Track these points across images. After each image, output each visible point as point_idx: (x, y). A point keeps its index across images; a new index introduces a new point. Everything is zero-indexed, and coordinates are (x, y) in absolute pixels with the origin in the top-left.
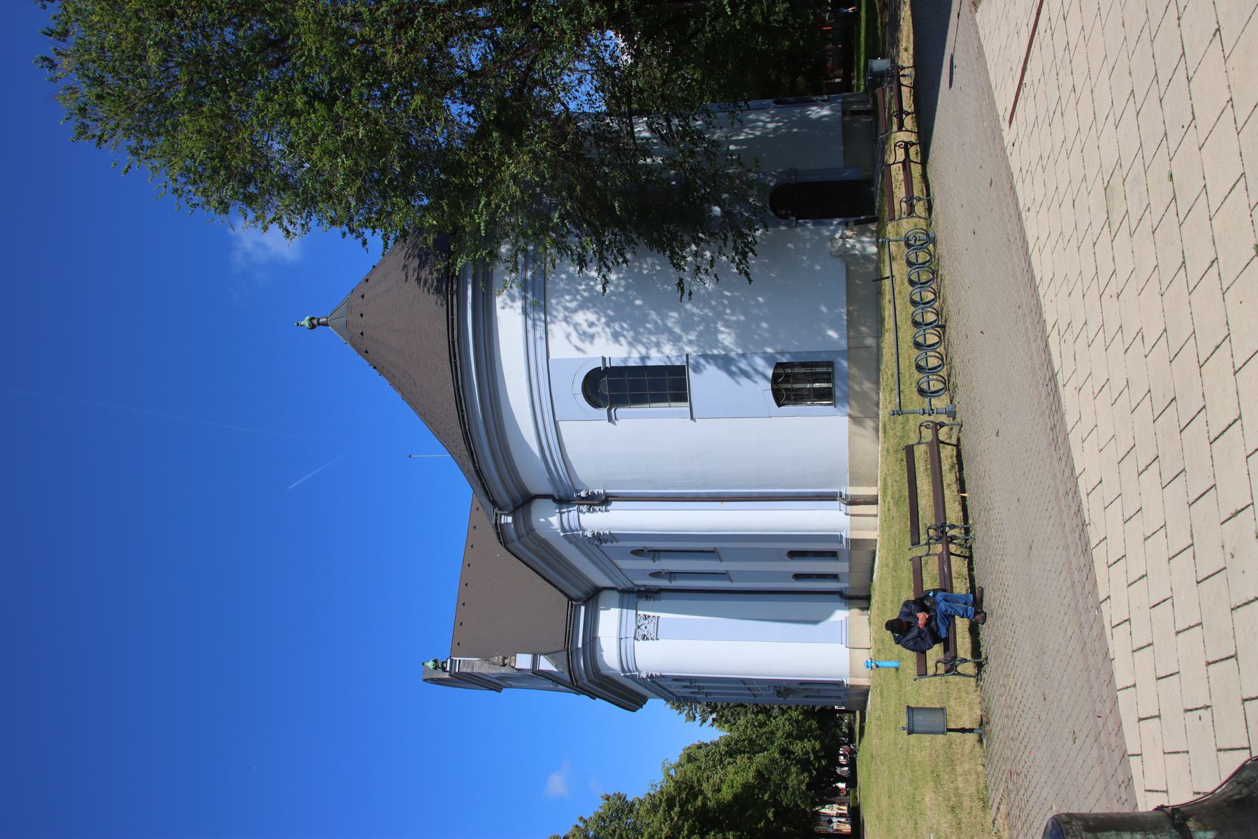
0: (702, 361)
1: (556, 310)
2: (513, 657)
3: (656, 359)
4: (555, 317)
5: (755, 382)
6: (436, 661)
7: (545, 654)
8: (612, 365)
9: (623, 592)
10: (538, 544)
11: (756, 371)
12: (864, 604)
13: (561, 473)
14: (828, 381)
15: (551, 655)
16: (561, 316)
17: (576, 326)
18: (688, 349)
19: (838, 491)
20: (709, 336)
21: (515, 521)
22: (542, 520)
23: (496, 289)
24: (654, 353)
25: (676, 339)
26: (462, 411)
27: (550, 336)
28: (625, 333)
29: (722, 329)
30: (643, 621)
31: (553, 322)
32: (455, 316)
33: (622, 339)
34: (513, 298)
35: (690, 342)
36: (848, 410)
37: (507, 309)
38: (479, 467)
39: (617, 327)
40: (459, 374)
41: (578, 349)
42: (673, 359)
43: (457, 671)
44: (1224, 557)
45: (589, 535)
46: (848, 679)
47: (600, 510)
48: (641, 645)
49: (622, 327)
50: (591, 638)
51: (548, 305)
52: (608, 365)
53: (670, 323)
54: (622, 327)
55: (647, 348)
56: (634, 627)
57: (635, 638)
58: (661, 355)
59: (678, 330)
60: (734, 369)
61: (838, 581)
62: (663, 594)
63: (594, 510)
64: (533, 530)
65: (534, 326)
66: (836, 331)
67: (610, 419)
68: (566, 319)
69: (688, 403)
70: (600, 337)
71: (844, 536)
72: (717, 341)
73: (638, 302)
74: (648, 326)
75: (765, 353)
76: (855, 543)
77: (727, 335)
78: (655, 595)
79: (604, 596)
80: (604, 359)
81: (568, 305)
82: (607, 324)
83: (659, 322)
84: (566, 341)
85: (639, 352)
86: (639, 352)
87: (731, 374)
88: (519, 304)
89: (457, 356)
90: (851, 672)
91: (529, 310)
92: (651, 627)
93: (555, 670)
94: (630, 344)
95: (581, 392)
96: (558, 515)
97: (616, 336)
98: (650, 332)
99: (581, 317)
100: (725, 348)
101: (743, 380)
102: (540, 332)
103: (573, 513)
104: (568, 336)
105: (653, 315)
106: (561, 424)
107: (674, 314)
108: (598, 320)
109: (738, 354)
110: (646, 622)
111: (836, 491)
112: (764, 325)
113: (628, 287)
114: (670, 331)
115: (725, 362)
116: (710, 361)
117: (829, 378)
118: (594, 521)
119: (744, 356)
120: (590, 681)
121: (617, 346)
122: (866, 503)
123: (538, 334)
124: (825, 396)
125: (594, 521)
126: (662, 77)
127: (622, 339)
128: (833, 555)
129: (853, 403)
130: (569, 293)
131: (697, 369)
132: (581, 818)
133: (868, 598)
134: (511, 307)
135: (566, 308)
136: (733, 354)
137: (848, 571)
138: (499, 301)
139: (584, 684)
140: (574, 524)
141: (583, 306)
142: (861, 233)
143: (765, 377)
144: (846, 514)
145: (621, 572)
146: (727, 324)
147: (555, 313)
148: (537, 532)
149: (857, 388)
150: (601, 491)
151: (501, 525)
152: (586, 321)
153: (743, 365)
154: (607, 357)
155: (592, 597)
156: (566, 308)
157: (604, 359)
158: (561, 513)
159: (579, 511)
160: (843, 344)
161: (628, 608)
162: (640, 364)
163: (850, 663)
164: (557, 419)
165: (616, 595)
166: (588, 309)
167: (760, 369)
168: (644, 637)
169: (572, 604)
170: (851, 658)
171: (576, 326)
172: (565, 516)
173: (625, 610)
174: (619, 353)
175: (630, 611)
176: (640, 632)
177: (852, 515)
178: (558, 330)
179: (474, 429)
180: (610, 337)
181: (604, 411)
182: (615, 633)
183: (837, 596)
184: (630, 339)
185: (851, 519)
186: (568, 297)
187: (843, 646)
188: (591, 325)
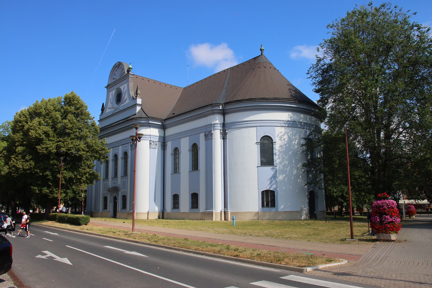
0: (275, 170)
1: (288, 130)
2: (140, 97)
3: (276, 158)
4: (286, 129)
5: (269, 185)
6: (132, 69)
7: (142, 108)
11: (272, 186)
12: (161, 217)
14: (266, 206)
16: (286, 131)
17: (284, 135)
18: (278, 167)
20: (283, 172)
21: (220, 110)
22: (217, 118)
23: (293, 113)
24: (277, 157)
25: (280, 163)
27: (281, 127)
28: (282, 149)
29: (283, 176)
30: (155, 143)
31: (285, 129)
32: (289, 101)
33: (280, 148)
34: (291, 117)
35: (280, 167)
36: (260, 211)
37: (288, 116)
39: (284, 147)
41: (278, 135)
42: (275, 162)
44: (385, 279)
45: (212, 132)
47: (221, 136)
48: (148, 142)
49: (284, 148)
51: (289, 128)
52: (274, 143)
53: (285, 161)
54: (284, 148)
55: (278, 155)
56: (154, 140)
57: (150, 141)
58: (277, 159)
59: (283, 164)
60: (273, 179)
62: (163, 151)
63: (221, 134)
64: (213, 114)
65: (286, 123)
66: (283, 208)
67: (257, 143)
68: (285, 132)
70: (281, 142)
72: (280, 175)
73: (290, 153)
74: (284, 156)
75: (277, 188)
76: (212, 213)
77: (282, 177)
79: (162, 131)
80: (275, 142)
81: (289, 133)
82: (285, 144)
83: (285, 159)
84: (280, 132)
85: (277, 153)
86: (277, 153)
87: (271, 178)
88: (289, 119)
89: (279, 101)
90: (139, 213)
91: (288, 122)
92: (153, 146)
94: (279, 150)
95: (266, 135)
96: (220, 123)
97: (281, 146)
98: (283, 156)
99: (286, 137)
100: (278, 177)
101: (269, 182)
102: (282, 125)
103: (220, 128)
104: (281, 132)
105: (287, 157)
106: (255, 128)
107: (287, 163)
108: (285, 141)
109: (277, 180)
110: (155, 145)
112: (284, 188)
113: (294, 150)
114: (283, 162)
115: (274, 176)
116: (275, 173)
117: (272, 206)
118: (217, 134)
119: (276, 182)
120: (135, 123)
121: (279, 147)
122: (225, 217)
123: (282, 124)
124: (263, 206)
125: (217, 134)
127: (280, 148)
128: (124, 206)
129: (262, 213)
130: (292, 134)
131: (272, 169)
132: (94, 118)
133: (163, 218)
134: (288, 117)
135: (288, 132)
136: (276, 179)
137: (181, 212)
138: (290, 113)
140: (216, 128)
141: (289, 137)
142: (306, 215)
143: (270, 188)
146: (285, 177)
147: (287, 129)
149: (267, 214)
150: (227, 137)
151: (220, 105)
152: (285, 138)
153: (274, 182)
154: (276, 143)
155: (163, 127)
156: (288, 132)
157: (275, 142)
158: (220, 124)
159: (221, 130)
160: (279, 210)
161: (159, 139)
162: (274, 153)
166: (288, 139)
167: (272, 187)
168: (150, 144)
169: (162, 120)
170: (144, 213)
171: (284, 135)
172: (219, 125)
173: (158, 138)
174: (277, 147)
175: (158, 139)
176: (153, 143)
177: (148, 213)
178: (283, 130)
180: (281, 144)
181: (259, 141)
182: (152, 134)
184: (280, 150)
185: (219, 213)
186: (291, 133)
187: (148, 210)
188: (284, 140)
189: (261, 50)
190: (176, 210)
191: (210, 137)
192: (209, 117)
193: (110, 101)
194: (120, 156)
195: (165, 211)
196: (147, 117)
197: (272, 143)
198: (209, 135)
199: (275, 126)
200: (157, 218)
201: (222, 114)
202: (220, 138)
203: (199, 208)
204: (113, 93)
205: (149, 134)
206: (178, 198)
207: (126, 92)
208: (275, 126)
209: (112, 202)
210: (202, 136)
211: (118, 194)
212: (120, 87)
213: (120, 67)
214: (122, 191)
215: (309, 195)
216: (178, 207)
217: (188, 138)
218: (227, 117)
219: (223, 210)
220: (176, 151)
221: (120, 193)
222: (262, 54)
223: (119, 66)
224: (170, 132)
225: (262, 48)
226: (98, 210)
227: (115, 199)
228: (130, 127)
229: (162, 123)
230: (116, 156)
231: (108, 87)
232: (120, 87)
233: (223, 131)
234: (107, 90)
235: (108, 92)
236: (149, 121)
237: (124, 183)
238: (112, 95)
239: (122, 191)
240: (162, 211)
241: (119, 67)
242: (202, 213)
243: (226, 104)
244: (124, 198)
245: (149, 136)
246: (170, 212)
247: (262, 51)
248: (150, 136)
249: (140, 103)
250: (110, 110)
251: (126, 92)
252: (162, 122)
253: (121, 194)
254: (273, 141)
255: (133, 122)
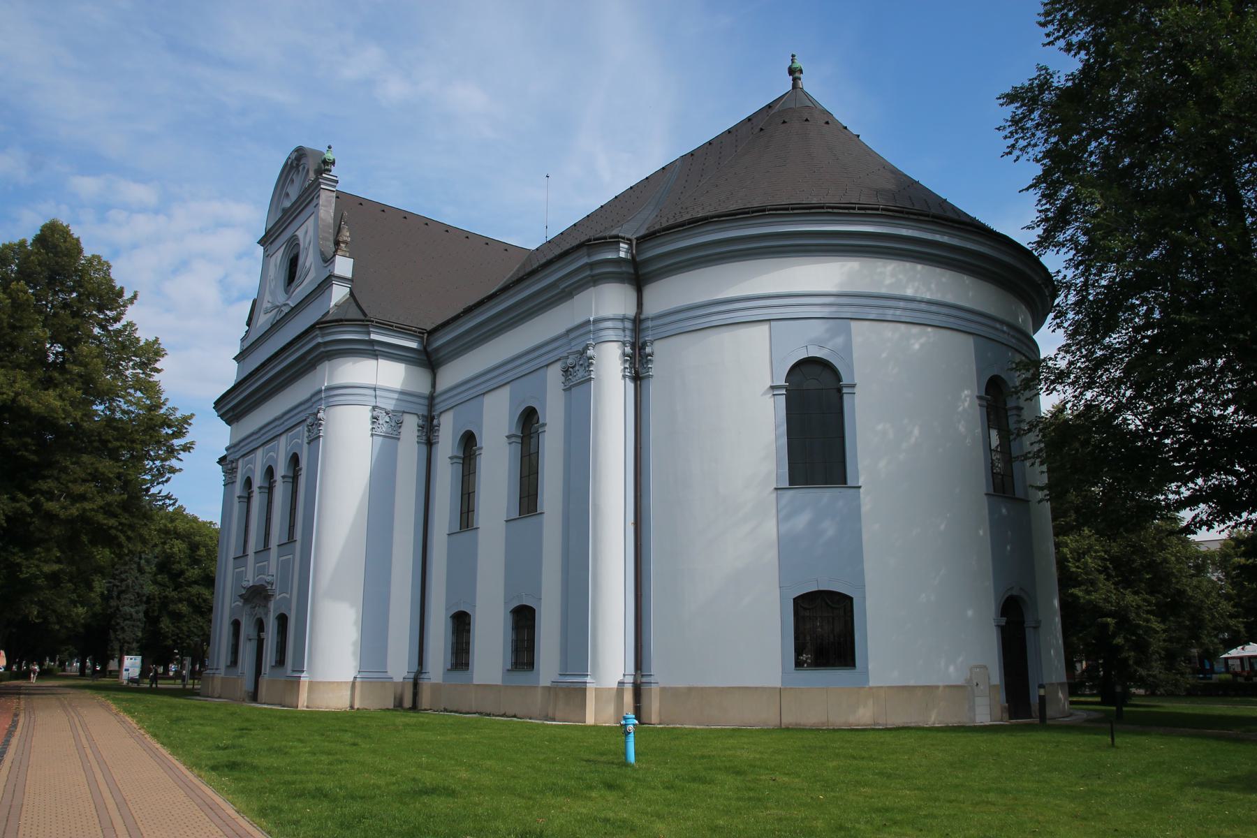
2: (348, 255)
7: (352, 293)
8: (845, 395)
9: (431, 399)
10: (566, 290)
13: (660, 330)
15: (352, 300)
19: (305, 669)
21: (619, 261)
26: (793, 209)
38: (659, 236)
40: (841, 211)
43: (322, 186)
45: (590, 352)
46: (307, 679)
47: (625, 368)
48: (365, 413)
50: (377, 352)
52: (845, 390)
57: (374, 408)
61: (228, 667)
62: (424, 448)
63: (625, 361)
64: (596, 280)
67: (773, 388)
69: (788, 486)
71: (303, 675)
76: (581, 691)
78: (424, 438)
80: (853, 386)
93: (332, 304)
106: (765, 327)
111: (589, 670)
120: (319, 345)
126: (43, 557)
128: (281, 662)
137: (476, 681)
139: (316, 336)
144: (355, 678)
145: (482, 394)
148: (592, 288)
151: (618, 243)
154: (856, 390)
163: (334, 682)
164: (772, 323)
165: (425, 389)
169: (423, 333)
175: (394, 402)
179: (674, 237)
182: (381, 383)
183: (415, 668)
189: (791, 71)
190: (459, 676)
191: (581, 373)
192: (581, 299)
193: (270, 286)
194: (281, 470)
195: (423, 676)
196: (362, 317)
197: (839, 390)
198: (577, 368)
199: (851, 319)
200: (392, 707)
201: (630, 283)
202: (621, 375)
203: (539, 670)
204: (279, 256)
205: (370, 381)
206: (467, 628)
207: (309, 244)
208: (851, 319)
209: (250, 640)
210: (554, 375)
211: (267, 614)
212: (296, 233)
213: (301, 168)
214: (278, 598)
215: (1003, 615)
216: (467, 665)
217: (507, 389)
218: (651, 292)
219: (630, 679)
220: (469, 442)
221: (272, 605)
222: (795, 86)
223: (297, 161)
224: (453, 374)
225: (797, 64)
226: (215, 667)
227: (260, 626)
228: (309, 358)
229: (421, 342)
230: (270, 472)
231: (266, 241)
232: (296, 233)
233: (633, 346)
234: (265, 251)
235: (267, 256)
236: (369, 333)
237: (285, 567)
238: (276, 265)
239: (278, 598)
240: (412, 675)
241: (298, 165)
242: (548, 688)
243: (642, 240)
244: (283, 620)
245: (372, 392)
246: (441, 681)
247: (797, 75)
248: (375, 389)
249: (348, 274)
250: (268, 315)
251: (309, 244)
252: (422, 338)
253: (274, 611)
254: (839, 378)
255: (313, 338)
